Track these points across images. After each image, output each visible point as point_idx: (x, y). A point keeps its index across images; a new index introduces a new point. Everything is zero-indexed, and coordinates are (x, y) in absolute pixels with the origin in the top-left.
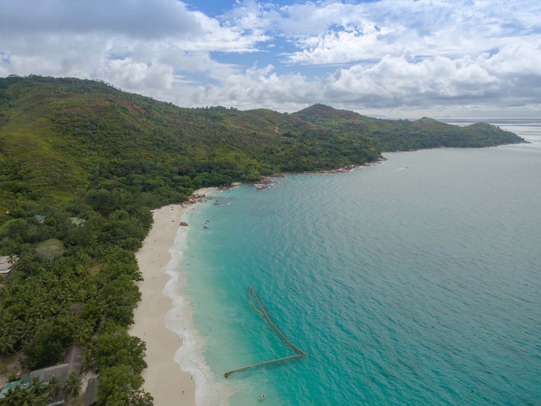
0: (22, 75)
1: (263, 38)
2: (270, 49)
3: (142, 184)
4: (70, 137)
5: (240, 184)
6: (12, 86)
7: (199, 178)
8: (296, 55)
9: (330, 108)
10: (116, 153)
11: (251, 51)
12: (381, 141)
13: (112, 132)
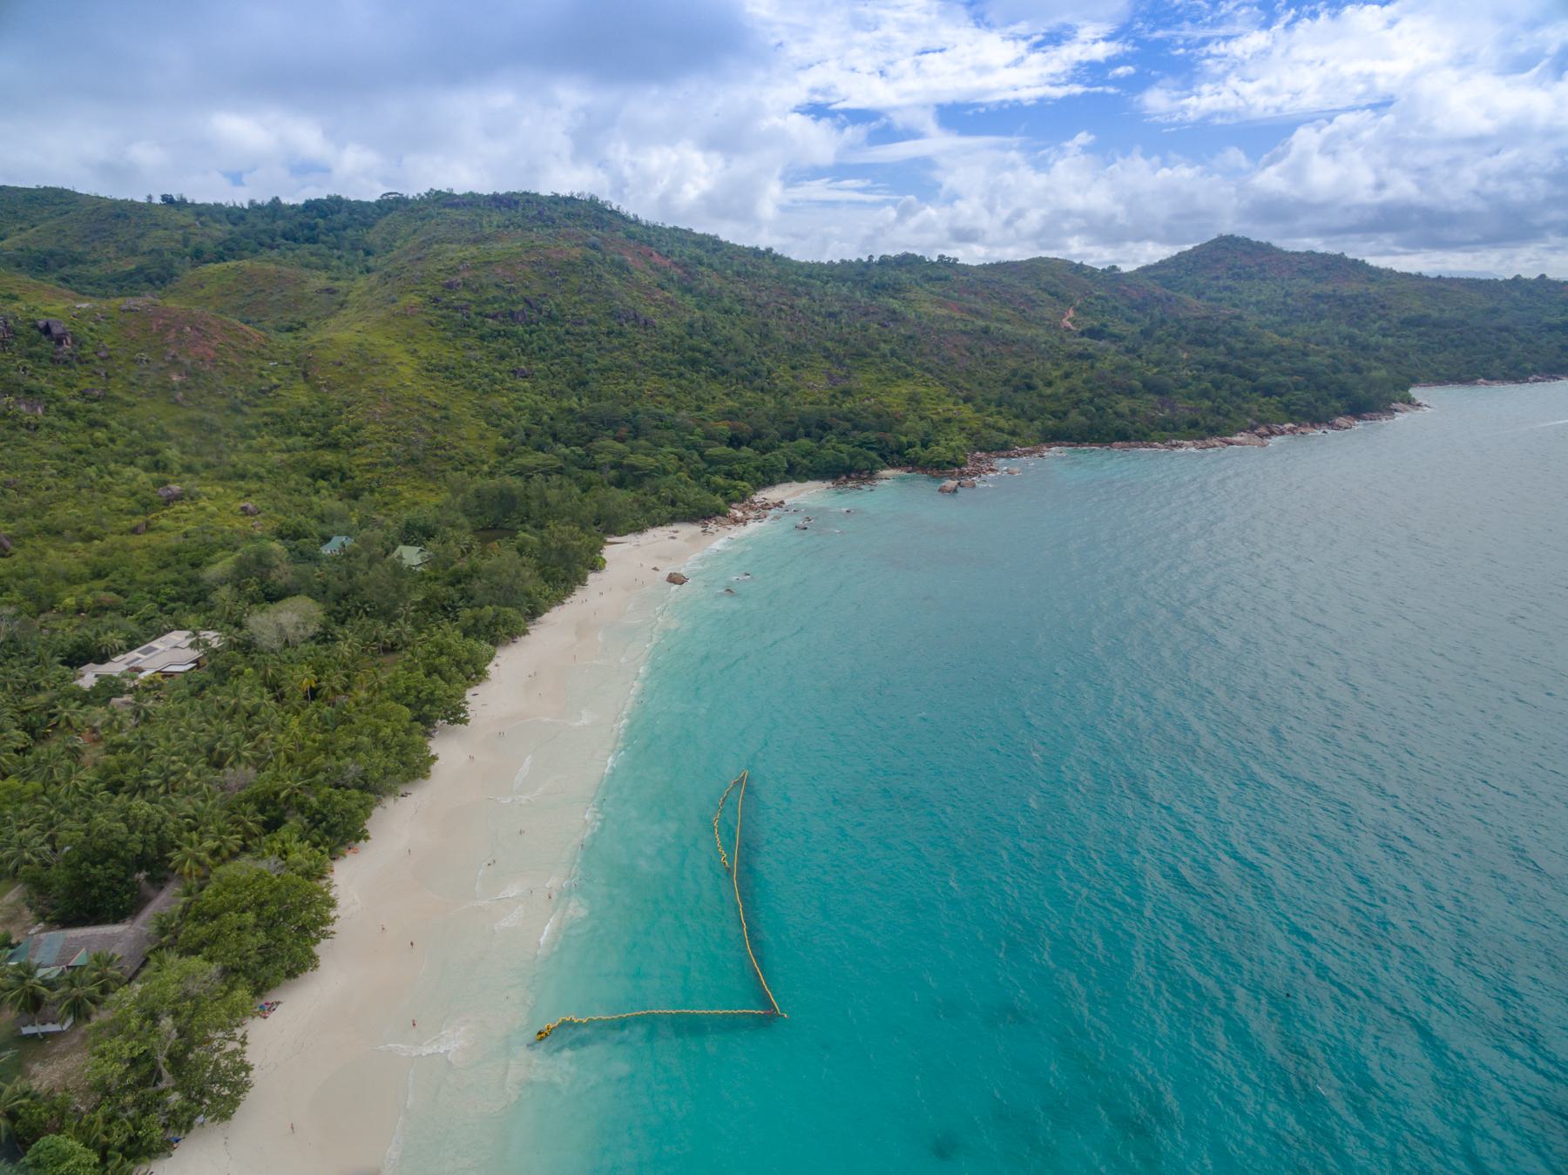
0: (411, 193)
1: (1101, 51)
2: (1117, 82)
3: (616, 466)
4: (470, 341)
5: (904, 473)
6: (383, 222)
7: (779, 457)
8: (1199, 95)
9: (1266, 249)
10: (580, 384)
11: (1060, 92)
12: (1423, 350)
13: (577, 330)
